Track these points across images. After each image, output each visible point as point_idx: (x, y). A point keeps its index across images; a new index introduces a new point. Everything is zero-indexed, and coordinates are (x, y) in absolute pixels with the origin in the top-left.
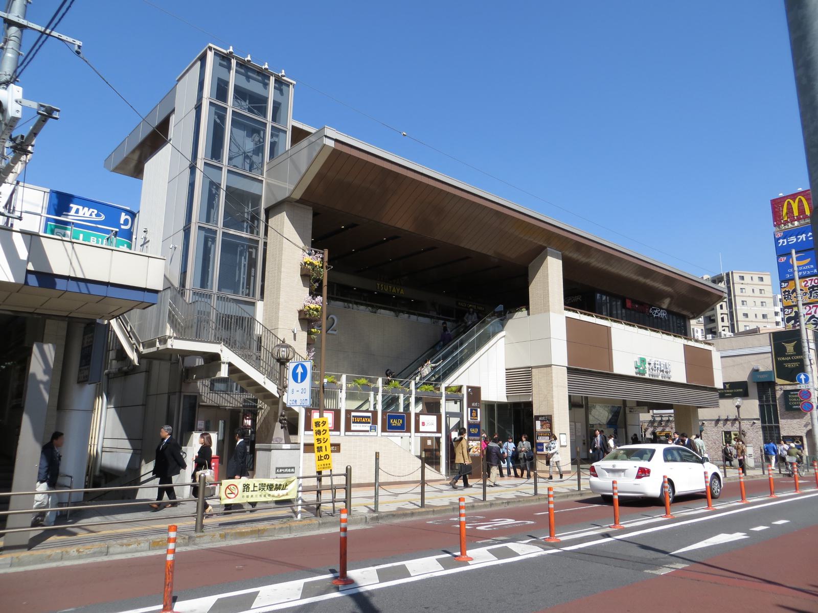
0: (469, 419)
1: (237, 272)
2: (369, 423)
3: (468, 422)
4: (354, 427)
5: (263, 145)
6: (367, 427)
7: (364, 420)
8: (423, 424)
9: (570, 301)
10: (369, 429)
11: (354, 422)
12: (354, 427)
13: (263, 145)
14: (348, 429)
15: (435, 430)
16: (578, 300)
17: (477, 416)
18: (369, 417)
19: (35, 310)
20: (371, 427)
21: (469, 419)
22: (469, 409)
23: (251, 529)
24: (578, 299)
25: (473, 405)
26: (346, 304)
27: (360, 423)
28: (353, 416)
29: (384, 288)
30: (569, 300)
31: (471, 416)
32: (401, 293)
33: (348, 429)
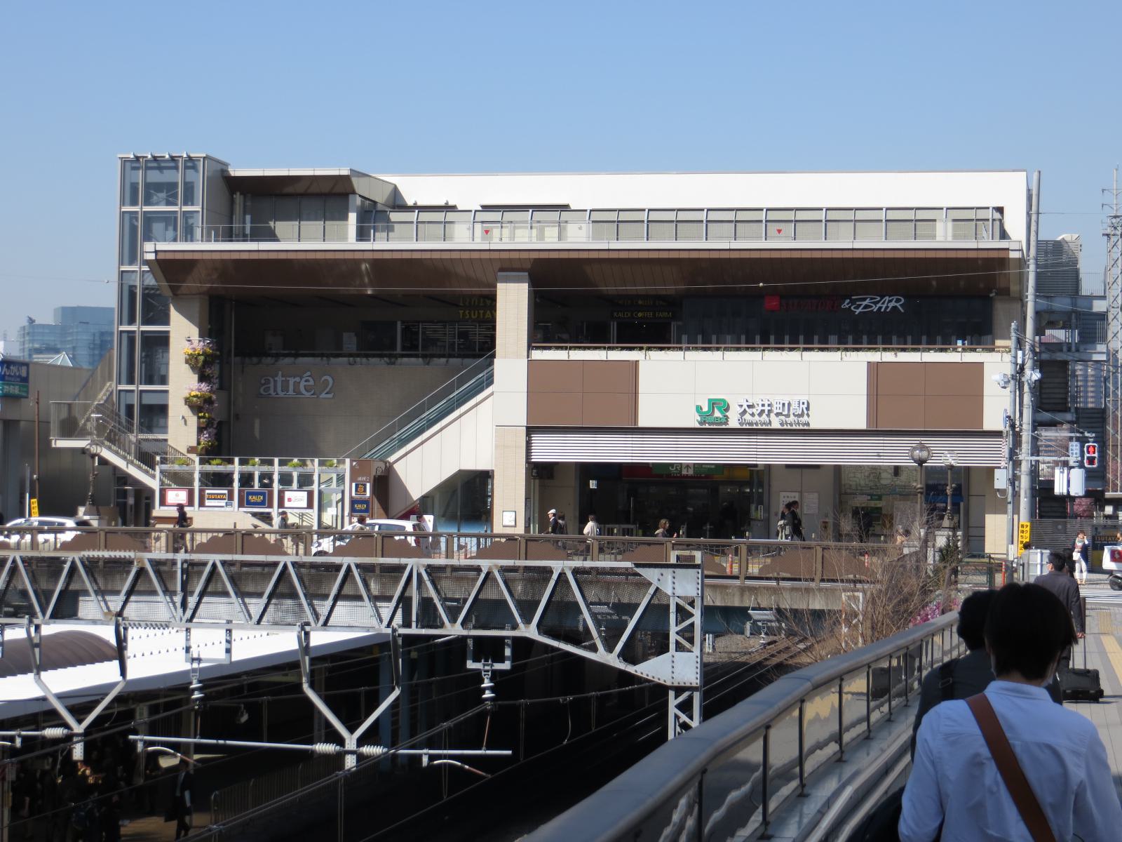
0: (353, 494)
1: (416, 421)
2: (225, 499)
3: (351, 497)
4: (208, 503)
5: (704, 701)
6: (223, 503)
7: (219, 497)
8: (290, 500)
9: (866, 307)
10: (224, 504)
11: (208, 499)
12: (208, 503)
13: (704, 701)
14: (202, 504)
15: (306, 506)
16: (895, 308)
17: (365, 491)
18: (224, 494)
19: (754, 609)
20: (226, 503)
21: (353, 494)
22: (354, 485)
23: (955, 629)
24: (891, 305)
25: (360, 479)
26: (351, 359)
27: (214, 499)
28: (208, 494)
29: (470, 315)
30: (864, 303)
31: (356, 490)
32: (487, 316)
33: (202, 504)
